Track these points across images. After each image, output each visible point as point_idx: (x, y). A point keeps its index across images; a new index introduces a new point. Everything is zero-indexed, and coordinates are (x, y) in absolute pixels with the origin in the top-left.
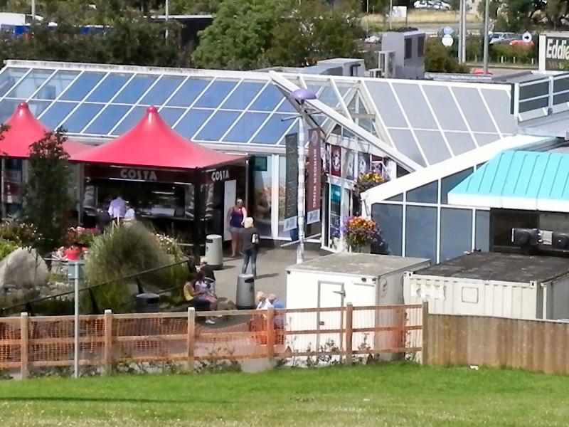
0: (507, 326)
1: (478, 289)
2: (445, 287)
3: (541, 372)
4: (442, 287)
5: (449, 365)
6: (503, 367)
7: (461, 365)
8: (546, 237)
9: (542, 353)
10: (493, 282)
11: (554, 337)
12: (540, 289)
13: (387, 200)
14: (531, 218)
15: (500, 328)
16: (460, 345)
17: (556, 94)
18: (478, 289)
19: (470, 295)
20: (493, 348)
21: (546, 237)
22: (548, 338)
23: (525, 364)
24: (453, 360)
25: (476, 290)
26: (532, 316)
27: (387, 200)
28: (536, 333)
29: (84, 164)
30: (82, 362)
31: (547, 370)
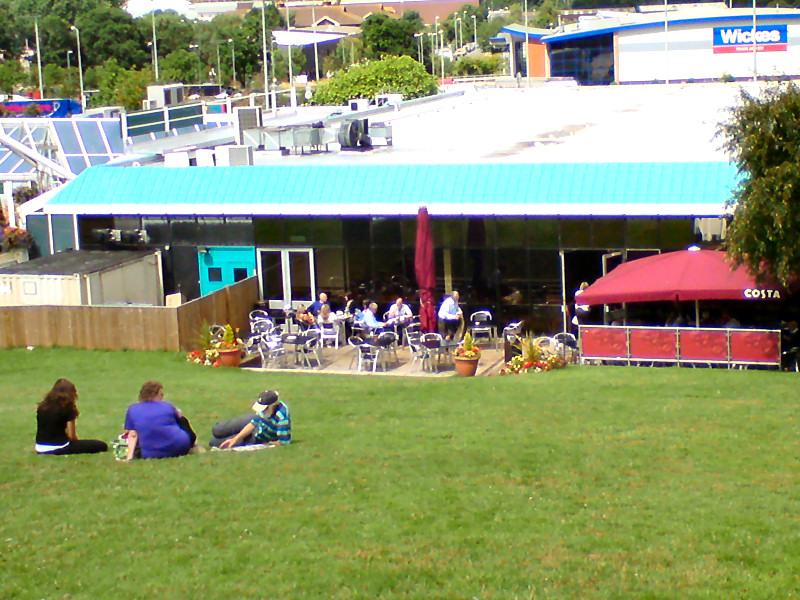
0: (55, 312)
1: (35, 284)
2: (11, 284)
3: (84, 348)
4: (8, 283)
5: (10, 347)
6: (55, 346)
7: (20, 347)
8: (116, 234)
9: (83, 332)
10: (46, 276)
11: (91, 318)
12: (83, 281)
13: (493, 155)
14: (108, 221)
15: (50, 313)
16: (18, 330)
17: (75, 126)
18: (35, 284)
19: (30, 288)
20: (46, 333)
21: (116, 234)
22: (87, 320)
23: (71, 343)
24: (14, 344)
25: (33, 285)
26: (77, 302)
27: (493, 155)
28: (77, 316)
29: (243, 127)
30: (678, 356)
31: (88, 347)
